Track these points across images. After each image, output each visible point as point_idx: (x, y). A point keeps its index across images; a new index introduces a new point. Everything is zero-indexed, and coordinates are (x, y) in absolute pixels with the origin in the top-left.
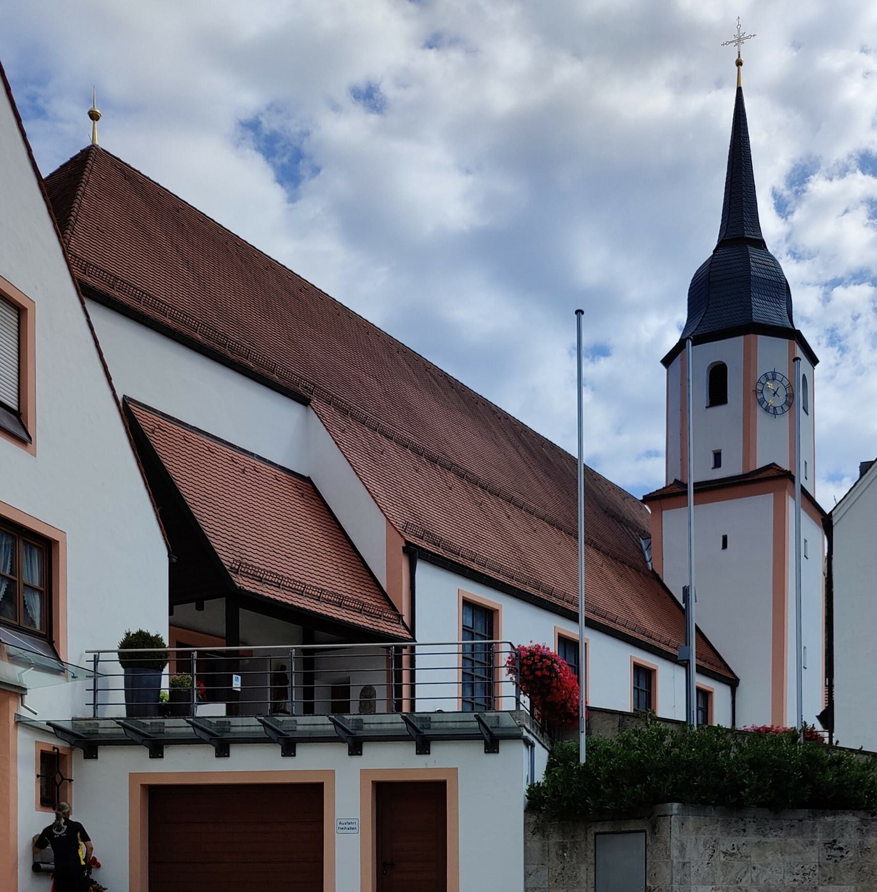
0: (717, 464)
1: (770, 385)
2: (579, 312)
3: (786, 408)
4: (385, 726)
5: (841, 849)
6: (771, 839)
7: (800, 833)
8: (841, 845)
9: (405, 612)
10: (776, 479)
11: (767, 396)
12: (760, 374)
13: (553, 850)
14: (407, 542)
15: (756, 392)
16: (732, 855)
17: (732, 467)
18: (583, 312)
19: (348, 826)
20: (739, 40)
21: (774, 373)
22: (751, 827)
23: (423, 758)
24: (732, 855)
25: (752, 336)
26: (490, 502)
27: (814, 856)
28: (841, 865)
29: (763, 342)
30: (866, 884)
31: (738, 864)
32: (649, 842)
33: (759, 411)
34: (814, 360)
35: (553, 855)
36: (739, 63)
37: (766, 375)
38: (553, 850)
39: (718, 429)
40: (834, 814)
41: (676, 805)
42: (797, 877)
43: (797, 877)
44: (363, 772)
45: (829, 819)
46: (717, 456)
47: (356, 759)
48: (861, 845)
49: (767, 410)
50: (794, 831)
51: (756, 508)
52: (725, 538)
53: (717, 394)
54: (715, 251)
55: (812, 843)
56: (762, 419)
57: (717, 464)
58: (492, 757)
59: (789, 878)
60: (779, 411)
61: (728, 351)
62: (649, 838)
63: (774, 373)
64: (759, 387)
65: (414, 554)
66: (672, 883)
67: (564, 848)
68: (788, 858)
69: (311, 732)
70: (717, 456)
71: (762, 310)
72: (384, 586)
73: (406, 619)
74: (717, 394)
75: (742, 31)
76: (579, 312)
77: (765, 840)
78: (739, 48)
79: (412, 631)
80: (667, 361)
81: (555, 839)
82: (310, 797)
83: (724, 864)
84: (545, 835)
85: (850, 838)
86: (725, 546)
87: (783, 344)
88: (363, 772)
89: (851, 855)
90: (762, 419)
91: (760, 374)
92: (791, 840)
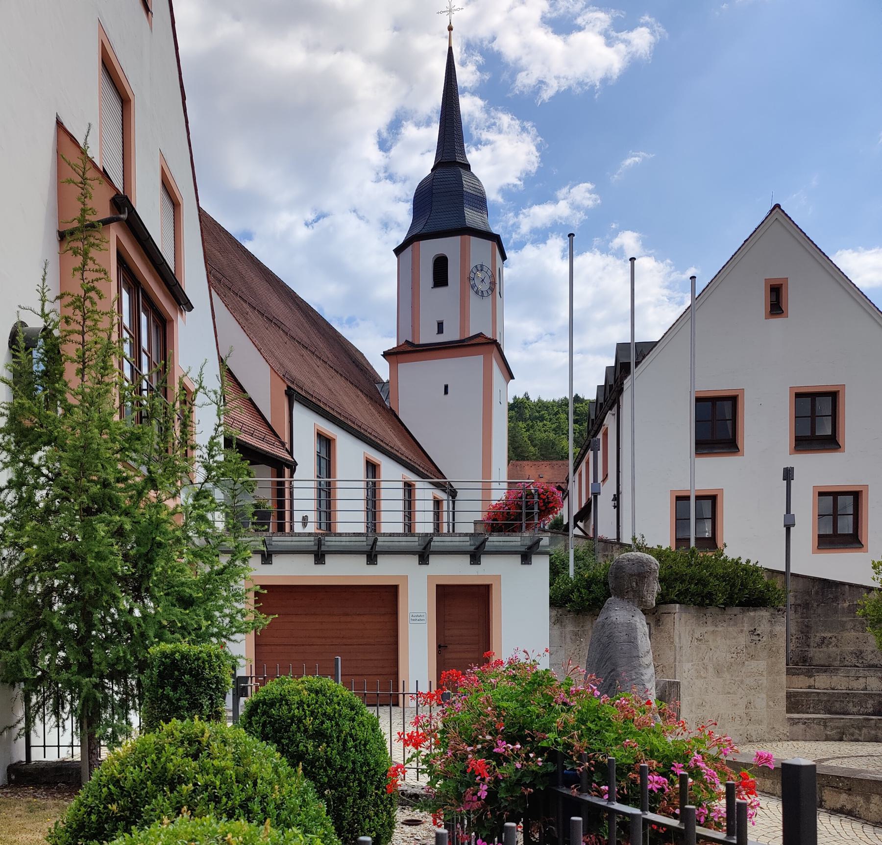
0: (440, 330)
1: (479, 274)
2: (571, 235)
3: (490, 292)
4: (447, 544)
5: (758, 635)
6: (720, 629)
7: (735, 625)
8: (759, 632)
9: (286, 440)
10: (487, 345)
11: (477, 282)
12: (472, 265)
13: (568, 636)
14: (288, 387)
15: (469, 278)
16: (700, 640)
17: (451, 334)
18: (574, 235)
19: (417, 618)
20: (450, 11)
21: (482, 266)
22: (710, 620)
23: (475, 567)
24: (700, 640)
25: (467, 236)
26: (304, 352)
27: (743, 640)
28: (759, 646)
29: (474, 240)
30: (774, 659)
31: (703, 647)
32: (653, 631)
33: (472, 293)
34: (504, 258)
35: (568, 640)
36: (450, 29)
37: (476, 267)
38: (568, 636)
39: (439, 304)
40: (755, 610)
41: (678, 605)
42: (734, 656)
43: (734, 656)
44: (429, 577)
45: (752, 614)
46: (440, 325)
47: (424, 567)
48: (771, 632)
49: (477, 292)
50: (732, 623)
51: (469, 366)
52: (446, 387)
53: (440, 278)
54: (432, 170)
55: (742, 631)
56: (474, 301)
57: (440, 330)
58: (526, 567)
59: (729, 656)
60: (485, 294)
61: (448, 246)
62: (653, 628)
63: (482, 266)
64: (472, 275)
65: (292, 395)
66: (675, 661)
67: (576, 634)
68: (728, 642)
69: (389, 547)
70: (440, 325)
71: (472, 217)
72: (269, 420)
73: (287, 446)
74: (440, 278)
75: (453, 5)
76: (571, 235)
77: (716, 629)
78: (450, 17)
79: (291, 453)
80: (398, 251)
81: (570, 628)
82: (387, 596)
83: (697, 647)
84: (563, 626)
85: (764, 628)
86: (446, 392)
87: (488, 244)
88: (429, 577)
89: (764, 639)
90: (474, 301)
91: (472, 265)
92: (730, 629)
